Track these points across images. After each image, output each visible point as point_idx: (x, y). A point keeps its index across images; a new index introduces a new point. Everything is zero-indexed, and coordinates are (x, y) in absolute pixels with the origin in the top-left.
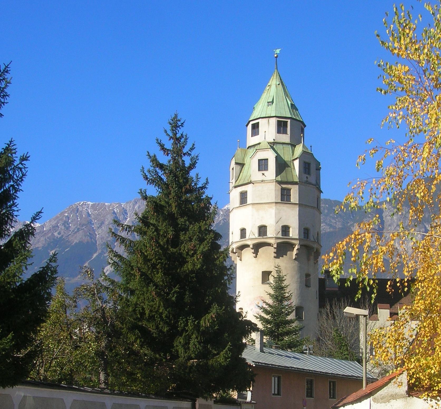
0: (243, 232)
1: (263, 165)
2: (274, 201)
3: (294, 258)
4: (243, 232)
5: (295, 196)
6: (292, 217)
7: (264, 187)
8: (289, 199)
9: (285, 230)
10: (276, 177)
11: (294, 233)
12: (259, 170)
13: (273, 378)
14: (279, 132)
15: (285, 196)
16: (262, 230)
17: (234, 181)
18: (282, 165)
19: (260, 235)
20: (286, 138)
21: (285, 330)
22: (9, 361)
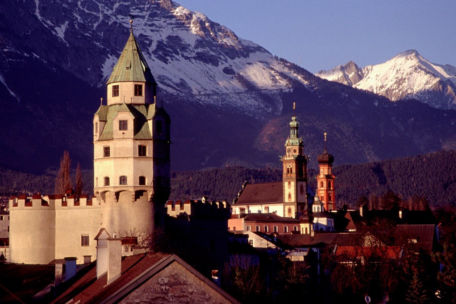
0: (107, 180)
1: (123, 125)
2: (133, 80)
3: (149, 200)
4: (107, 180)
5: (149, 151)
6: (148, 168)
7: (125, 143)
8: (144, 154)
9: (142, 180)
10: (134, 135)
11: (149, 181)
12: (120, 129)
13: (291, 131)
14: (136, 94)
15: (142, 151)
16: (123, 180)
17: (98, 134)
18: (140, 121)
19: (121, 184)
20: (141, 100)
21: (175, 91)
22: (437, 293)
